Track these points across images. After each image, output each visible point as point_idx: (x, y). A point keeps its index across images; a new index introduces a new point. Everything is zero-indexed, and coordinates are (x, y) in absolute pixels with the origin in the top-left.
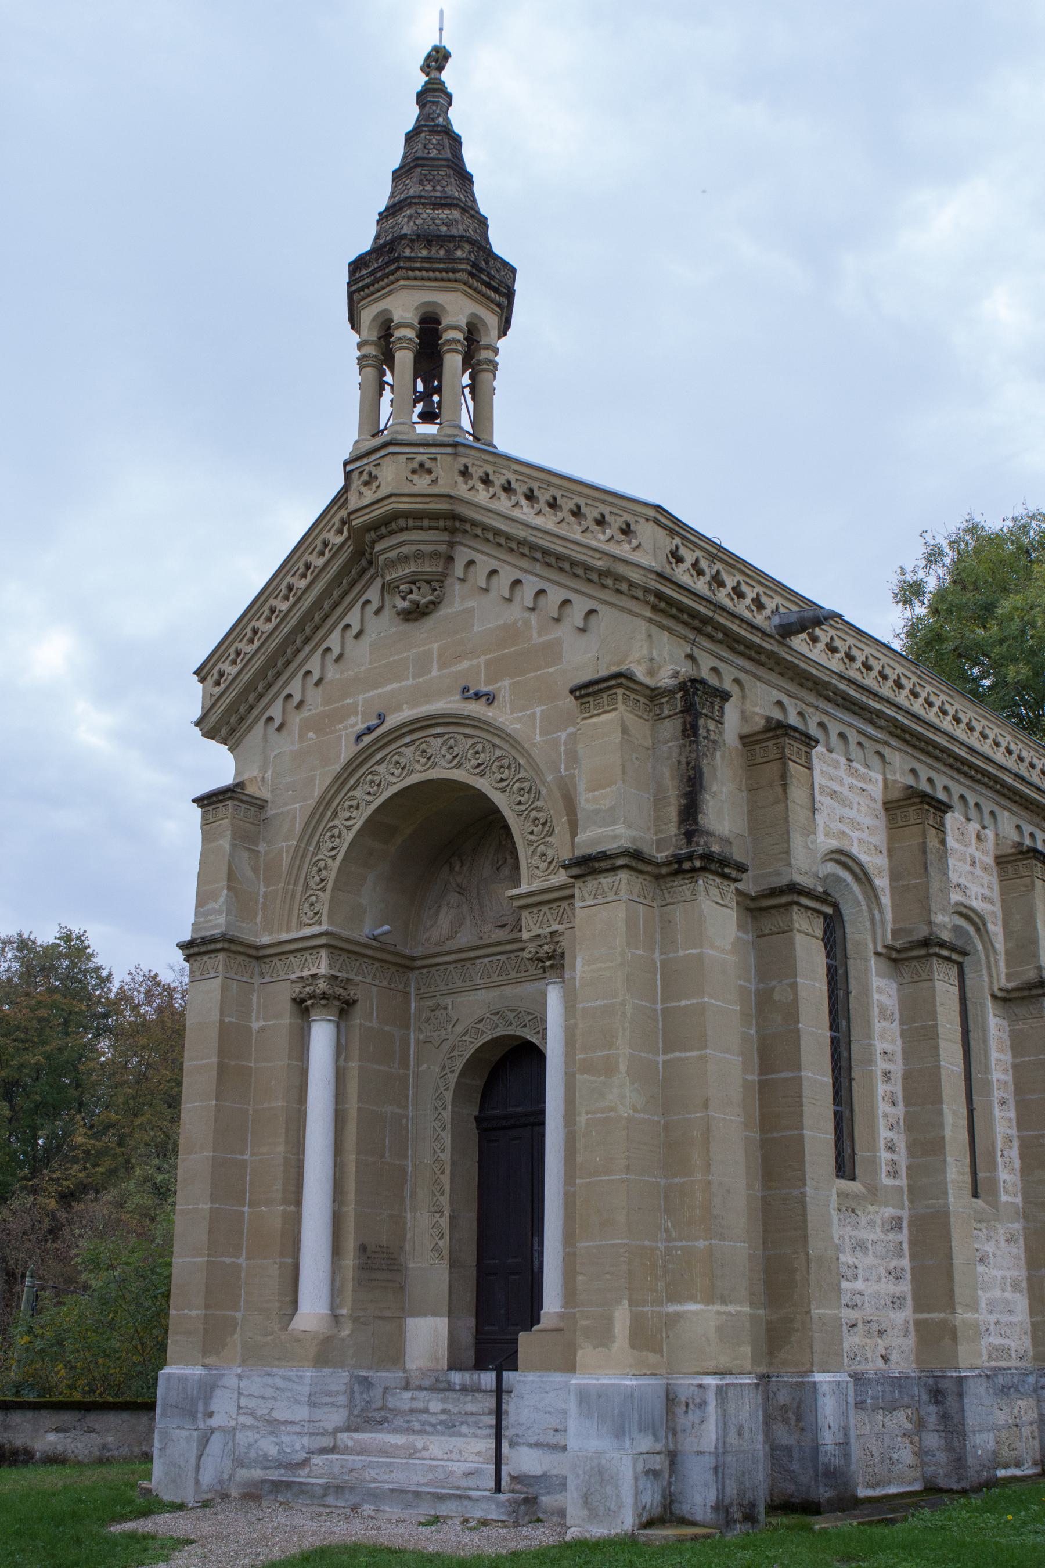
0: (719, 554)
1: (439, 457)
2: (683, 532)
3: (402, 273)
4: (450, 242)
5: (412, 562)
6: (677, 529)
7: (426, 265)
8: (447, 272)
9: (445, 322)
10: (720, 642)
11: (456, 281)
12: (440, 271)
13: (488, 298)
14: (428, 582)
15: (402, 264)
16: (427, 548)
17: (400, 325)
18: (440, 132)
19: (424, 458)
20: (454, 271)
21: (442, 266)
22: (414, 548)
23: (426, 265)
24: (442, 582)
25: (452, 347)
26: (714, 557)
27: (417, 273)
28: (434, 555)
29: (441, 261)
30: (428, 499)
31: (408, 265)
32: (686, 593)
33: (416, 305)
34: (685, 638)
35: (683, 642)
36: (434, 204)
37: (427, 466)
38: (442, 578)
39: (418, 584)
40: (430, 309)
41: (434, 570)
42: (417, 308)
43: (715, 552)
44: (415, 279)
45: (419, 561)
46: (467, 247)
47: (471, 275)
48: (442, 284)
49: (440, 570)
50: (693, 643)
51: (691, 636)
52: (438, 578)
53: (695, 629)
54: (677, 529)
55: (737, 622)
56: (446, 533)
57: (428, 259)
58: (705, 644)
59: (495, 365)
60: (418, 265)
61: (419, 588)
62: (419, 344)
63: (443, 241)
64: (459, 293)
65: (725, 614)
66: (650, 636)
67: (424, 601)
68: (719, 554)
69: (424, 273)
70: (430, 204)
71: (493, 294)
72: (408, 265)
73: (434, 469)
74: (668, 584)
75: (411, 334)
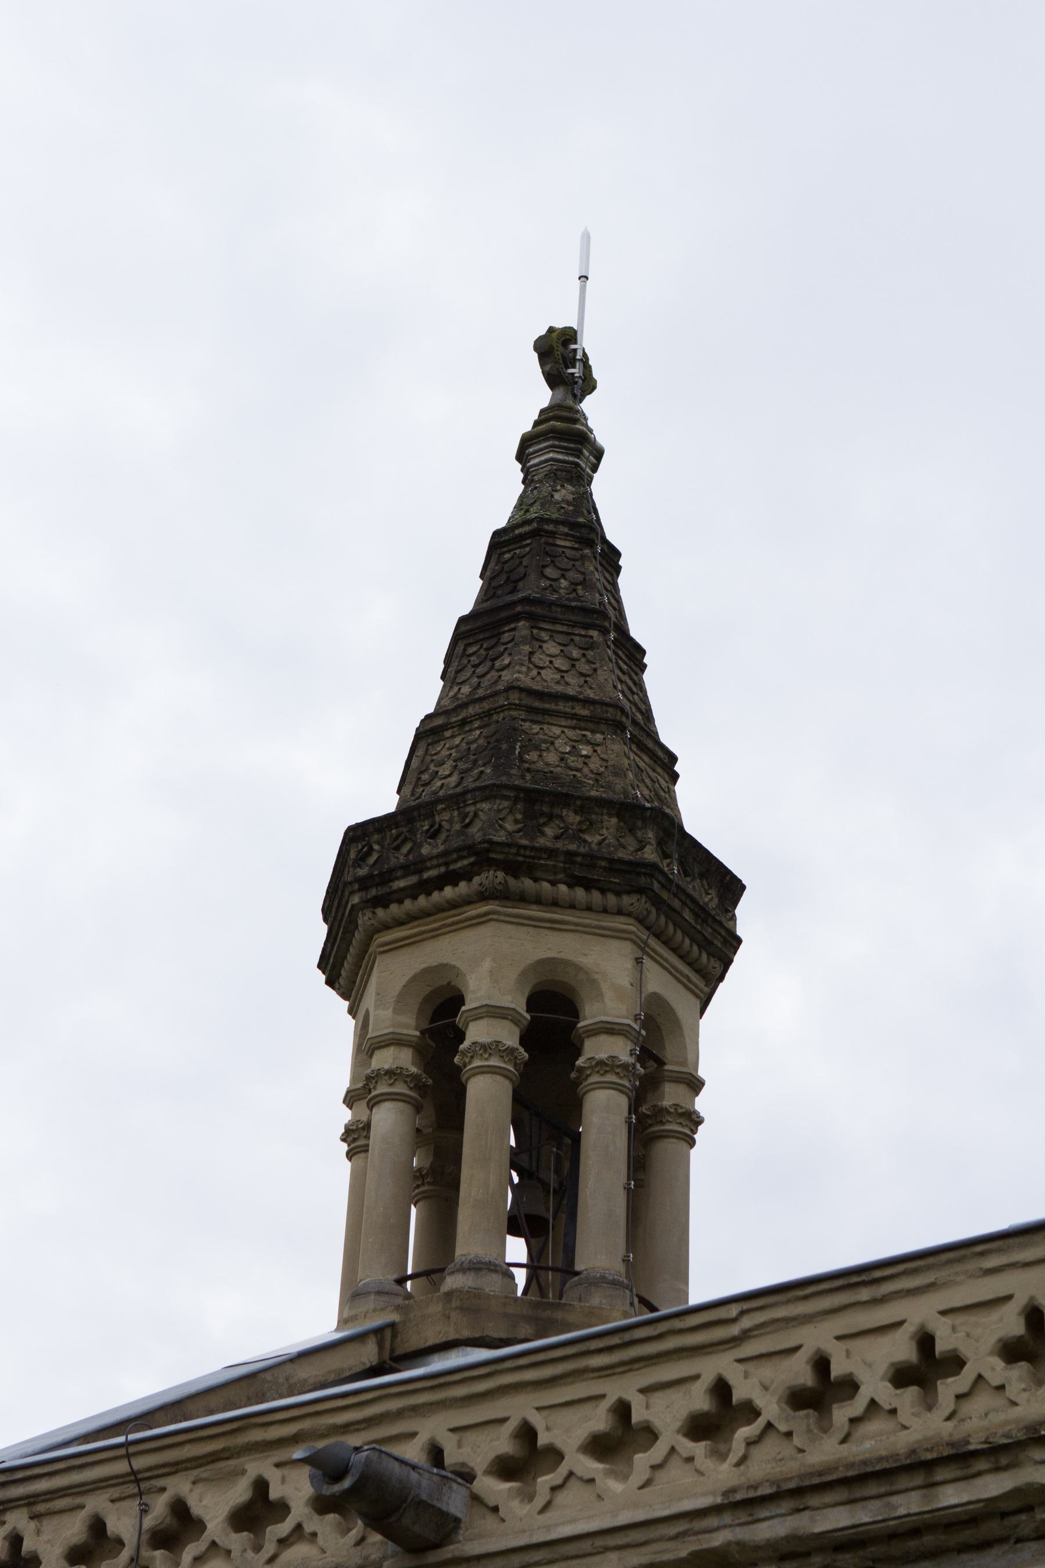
9: (591, 1014)
13: (453, 905)
17: (610, 1029)
26: (135, 1477)
43: (121, 1467)
68: (139, 1463)
71: (449, 892)
75: (509, 1036)
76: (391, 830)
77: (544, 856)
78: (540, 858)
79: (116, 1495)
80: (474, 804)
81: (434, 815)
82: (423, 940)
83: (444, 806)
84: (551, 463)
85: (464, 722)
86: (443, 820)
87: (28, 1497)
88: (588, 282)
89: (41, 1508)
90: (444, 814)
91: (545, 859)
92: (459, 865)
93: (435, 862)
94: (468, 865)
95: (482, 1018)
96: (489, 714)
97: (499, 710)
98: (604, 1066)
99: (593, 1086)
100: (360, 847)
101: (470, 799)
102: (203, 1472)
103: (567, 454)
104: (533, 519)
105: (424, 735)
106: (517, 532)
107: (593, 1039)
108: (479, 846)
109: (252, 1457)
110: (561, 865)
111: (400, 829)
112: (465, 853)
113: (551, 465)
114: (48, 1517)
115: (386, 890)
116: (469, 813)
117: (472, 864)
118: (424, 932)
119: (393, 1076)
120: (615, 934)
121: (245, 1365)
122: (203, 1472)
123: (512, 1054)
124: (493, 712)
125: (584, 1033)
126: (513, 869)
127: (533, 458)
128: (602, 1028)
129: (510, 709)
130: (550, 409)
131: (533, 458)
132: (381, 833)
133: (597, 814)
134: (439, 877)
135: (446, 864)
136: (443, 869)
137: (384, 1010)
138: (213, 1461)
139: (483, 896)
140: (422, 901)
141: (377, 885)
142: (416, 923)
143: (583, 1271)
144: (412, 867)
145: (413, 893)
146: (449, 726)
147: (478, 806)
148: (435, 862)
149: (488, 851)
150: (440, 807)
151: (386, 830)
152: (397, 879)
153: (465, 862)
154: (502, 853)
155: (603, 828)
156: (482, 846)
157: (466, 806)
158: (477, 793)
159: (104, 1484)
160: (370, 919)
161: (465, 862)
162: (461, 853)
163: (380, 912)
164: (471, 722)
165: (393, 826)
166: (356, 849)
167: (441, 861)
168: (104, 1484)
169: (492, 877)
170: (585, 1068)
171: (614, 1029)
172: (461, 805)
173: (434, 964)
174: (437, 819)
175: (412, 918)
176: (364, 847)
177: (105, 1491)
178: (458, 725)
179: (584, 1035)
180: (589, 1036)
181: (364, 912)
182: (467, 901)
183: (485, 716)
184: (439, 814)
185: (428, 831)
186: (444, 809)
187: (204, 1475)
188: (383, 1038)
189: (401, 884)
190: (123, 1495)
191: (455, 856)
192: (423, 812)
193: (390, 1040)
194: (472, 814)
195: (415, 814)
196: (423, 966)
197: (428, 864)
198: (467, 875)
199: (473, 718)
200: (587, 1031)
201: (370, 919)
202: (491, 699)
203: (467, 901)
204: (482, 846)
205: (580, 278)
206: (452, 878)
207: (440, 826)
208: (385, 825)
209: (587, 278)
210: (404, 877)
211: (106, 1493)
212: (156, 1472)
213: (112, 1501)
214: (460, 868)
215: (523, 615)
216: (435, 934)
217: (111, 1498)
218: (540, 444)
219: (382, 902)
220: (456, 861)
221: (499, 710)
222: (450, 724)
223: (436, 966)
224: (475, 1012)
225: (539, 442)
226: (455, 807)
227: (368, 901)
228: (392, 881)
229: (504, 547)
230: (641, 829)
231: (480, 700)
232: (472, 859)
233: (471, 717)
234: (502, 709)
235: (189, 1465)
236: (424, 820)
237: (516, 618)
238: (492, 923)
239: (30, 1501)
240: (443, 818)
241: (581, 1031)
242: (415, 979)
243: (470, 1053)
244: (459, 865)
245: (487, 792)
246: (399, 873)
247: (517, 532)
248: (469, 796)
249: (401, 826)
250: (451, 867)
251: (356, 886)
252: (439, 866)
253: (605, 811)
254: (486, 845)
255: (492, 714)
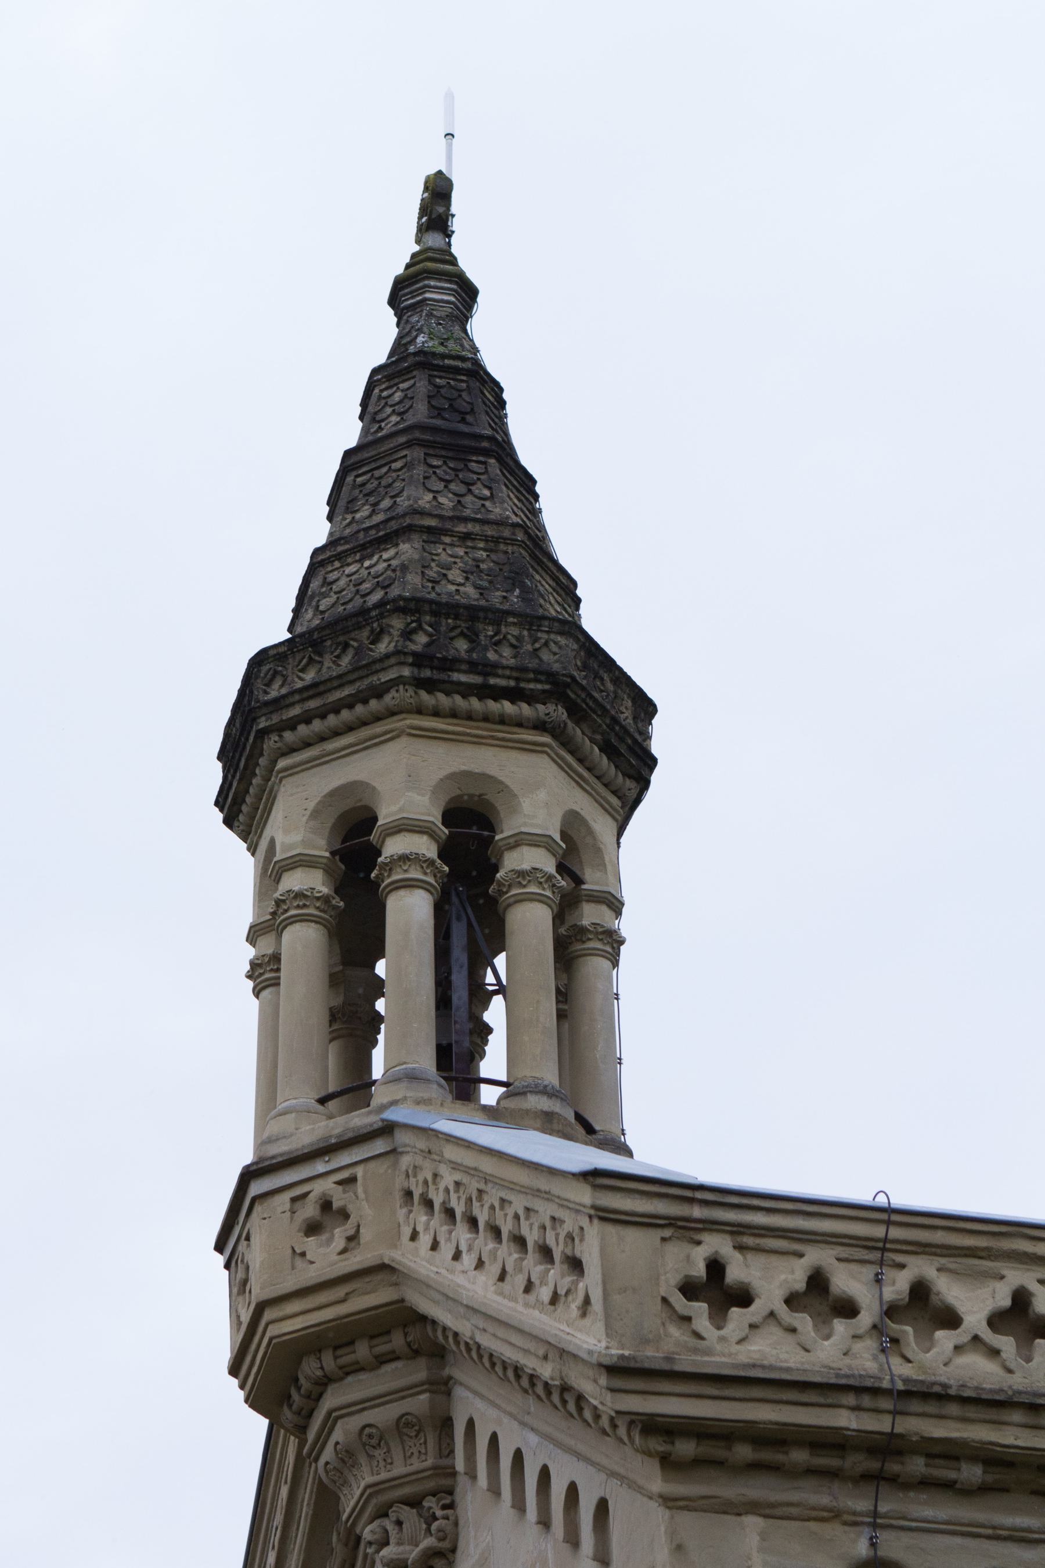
0: (895, 1233)
1: (359, 1171)
2: (731, 1216)
3: (271, 743)
4: (359, 627)
5: (363, 1459)
6: (697, 1212)
7: (313, 704)
8: (365, 702)
10: (984, 1489)
11: (392, 713)
12: (349, 704)
13: (503, 720)
14: (414, 1502)
15: (263, 723)
16: (382, 1416)
18: (408, 370)
19: (327, 1186)
20: (379, 692)
21: (347, 691)
22: (355, 1423)
23: (313, 704)
24: (451, 1492)
25: (533, 889)
26: (882, 1246)
27: (302, 729)
28: (404, 1426)
29: (342, 680)
30: (340, 1292)
31: (275, 719)
32: (756, 1392)
33: (311, 805)
34: (834, 1515)
35: (834, 1530)
36: (363, 547)
37: (336, 1205)
38: (446, 1482)
39: (393, 1516)
40: (349, 804)
41: (416, 1465)
42: (315, 814)
43: (879, 1231)
44: (436, 713)
45: (378, 1453)
46: (397, 623)
47: (421, 684)
48: (378, 728)
49: (429, 1462)
50: (876, 1522)
51: (860, 1504)
52: (431, 1485)
53: (867, 1477)
54: (697, 1212)
55: (1017, 1416)
56: (422, 1362)
57: (314, 689)
58: (928, 1512)
59: (614, 942)
60: (296, 711)
61: (399, 1523)
62: (449, 875)
63: (346, 631)
64: (404, 740)
65: (954, 1409)
66: (679, 1548)
67: (413, 1554)
68: (895, 1233)
69: (317, 725)
70: (352, 551)
71: (507, 707)
72: (275, 719)
73: (351, 1208)
74: (666, 1386)
76: (447, 619)
77: (599, 713)
78: (595, 712)
79: (844, 1255)
80: (548, 632)
81: (501, 624)
82: (462, 741)
83: (515, 620)
84: (452, 306)
85: (466, 537)
86: (509, 633)
87: (740, 1225)
88: (454, 140)
89: (749, 1241)
90: (512, 628)
91: (598, 715)
92: (532, 686)
93: (508, 672)
94: (541, 690)
95: (539, 846)
96: (496, 540)
97: (509, 542)
98: (523, 876)
99: (597, 952)
100: (409, 620)
101: (545, 627)
102: (951, 1262)
103: (462, 304)
104: (468, 358)
105: (419, 529)
106: (447, 361)
107: (593, 905)
108: (561, 678)
109: (1011, 1265)
110: (605, 727)
111: (458, 622)
112: (543, 678)
113: (451, 308)
114: (753, 1252)
115: (443, 676)
116: (540, 638)
117: (544, 691)
118: (468, 735)
119: (407, 861)
120: (610, 810)
121: (468, 1124)
122: (951, 1262)
123: (499, 886)
124: (502, 541)
125: (586, 895)
126: (574, 711)
127: (432, 292)
128: (606, 898)
129: (520, 546)
130: (441, 251)
131: (432, 292)
132: (436, 616)
133: (622, 690)
134: (469, 686)
135: (517, 679)
136: (512, 683)
137: (418, 795)
138: (966, 1256)
139: (540, 726)
140: (475, 703)
141: (432, 668)
142: (455, 721)
143: (599, 1131)
144: (480, 667)
145: (466, 691)
146: (449, 533)
147: (552, 636)
148: (508, 672)
149: (567, 685)
150: (511, 620)
151: (443, 616)
152: (459, 671)
153: (539, 686)
154: (576, 693)
155: (622, 705)
156: (565, 679)
157: (538, 630)
158: (556, 624)
159: (834, 1240)
160: (411, 697)
161: (539, 686)
162: (539, 676)
163: (423, 694)
164: (474, 539)
165: (453, 617)
166: (405, 621)
167: (515, 674)
168: (834, 1240)
169: (557, 712)
170: (588, 930)
171: (612, 903)
172: (534, 628)
173: (477, 771)
174: (503, 629)
175: (454, 714)
176: (412, 622)
177: (833, 1246)
178: (459, 537)
179: (584, 897)
180: (588, 901)
181: (407, 687)
182: (519, 723)
183: (492, 541)
184: (506, 626)
185: (492, 637)
186: (514, 624)
187: (953, 1266)
188: (421, 824)
189: (463, 678)
190: (851, 1257)
191: (531, 676)
192: (490, 616)
193: (428, 828)
194: (543, 641)
195: (481, 614)
196: (463, 768)
197: (500, 672)
198: (530, 698)
199: (478, 537)
200: (590, 896)
201: (411, 697)
202: (495, 527)
203: (519, 723)
204: (565, 679)
205: (446, 135)
206: (514, 695)
207: (505, 637)
208: (444, 611)
209: (453, 136)
210: (465, 672)
211: (832, 1249)
212: (899, 1247)
213: (839, 1259)
214: (532, 690)
215: (414, 442)
216: (478, 741)
217: (837, 1256)
218: (440, 282)
219: (429, 686)
220: (529, 681)
221: (509, 542)
222: (452, 531)
223: (478, 773)
224: (535, 838)
225: (440, 280)
226: (527, 627)
227: (415, 679)
228: (452, 670)
229: (436, 370)
230: (642, 721)
231: (482, 522)
232: (547, 687)
233: (476, 535)
234: (514, 542)
235: (938, 1251)
236: (489, 624)
237: (486, 452)
238: (545, 756)
239: (736, 1230)
240: (510, 632)
241: (583, 892)
242: (452, 776)
243: (529, 876)
244: (532, 686)
245: (567, 628)
246: (464, 667)
247: (447, 361)
248: (546, 623)
249: (460, 620)
250: (522, 685)
251: (410, 660)
252: (509, 678)
253: (627, 691)
254: (569, 680)
255: (501, 542)
